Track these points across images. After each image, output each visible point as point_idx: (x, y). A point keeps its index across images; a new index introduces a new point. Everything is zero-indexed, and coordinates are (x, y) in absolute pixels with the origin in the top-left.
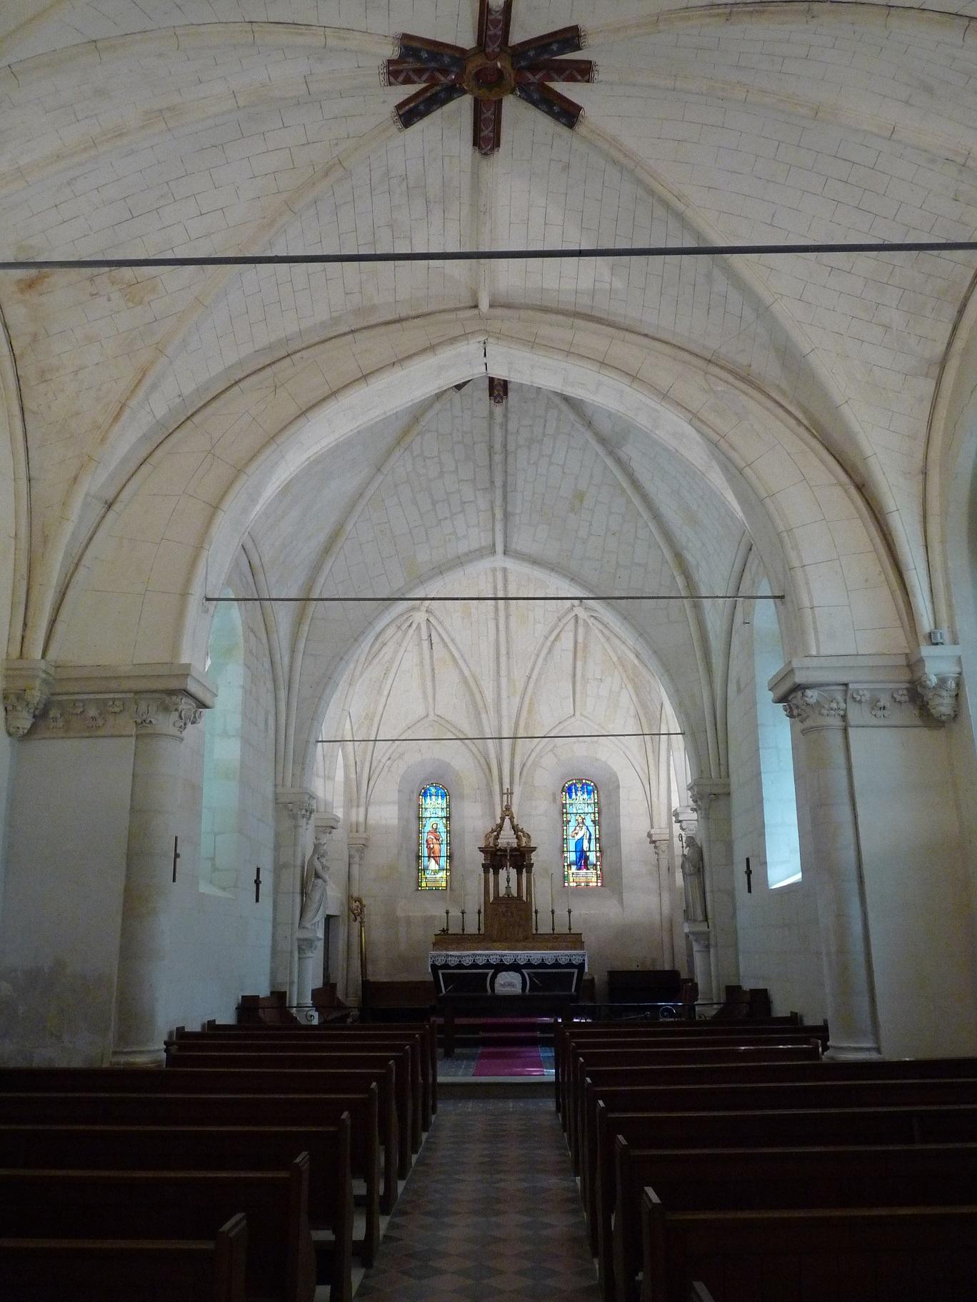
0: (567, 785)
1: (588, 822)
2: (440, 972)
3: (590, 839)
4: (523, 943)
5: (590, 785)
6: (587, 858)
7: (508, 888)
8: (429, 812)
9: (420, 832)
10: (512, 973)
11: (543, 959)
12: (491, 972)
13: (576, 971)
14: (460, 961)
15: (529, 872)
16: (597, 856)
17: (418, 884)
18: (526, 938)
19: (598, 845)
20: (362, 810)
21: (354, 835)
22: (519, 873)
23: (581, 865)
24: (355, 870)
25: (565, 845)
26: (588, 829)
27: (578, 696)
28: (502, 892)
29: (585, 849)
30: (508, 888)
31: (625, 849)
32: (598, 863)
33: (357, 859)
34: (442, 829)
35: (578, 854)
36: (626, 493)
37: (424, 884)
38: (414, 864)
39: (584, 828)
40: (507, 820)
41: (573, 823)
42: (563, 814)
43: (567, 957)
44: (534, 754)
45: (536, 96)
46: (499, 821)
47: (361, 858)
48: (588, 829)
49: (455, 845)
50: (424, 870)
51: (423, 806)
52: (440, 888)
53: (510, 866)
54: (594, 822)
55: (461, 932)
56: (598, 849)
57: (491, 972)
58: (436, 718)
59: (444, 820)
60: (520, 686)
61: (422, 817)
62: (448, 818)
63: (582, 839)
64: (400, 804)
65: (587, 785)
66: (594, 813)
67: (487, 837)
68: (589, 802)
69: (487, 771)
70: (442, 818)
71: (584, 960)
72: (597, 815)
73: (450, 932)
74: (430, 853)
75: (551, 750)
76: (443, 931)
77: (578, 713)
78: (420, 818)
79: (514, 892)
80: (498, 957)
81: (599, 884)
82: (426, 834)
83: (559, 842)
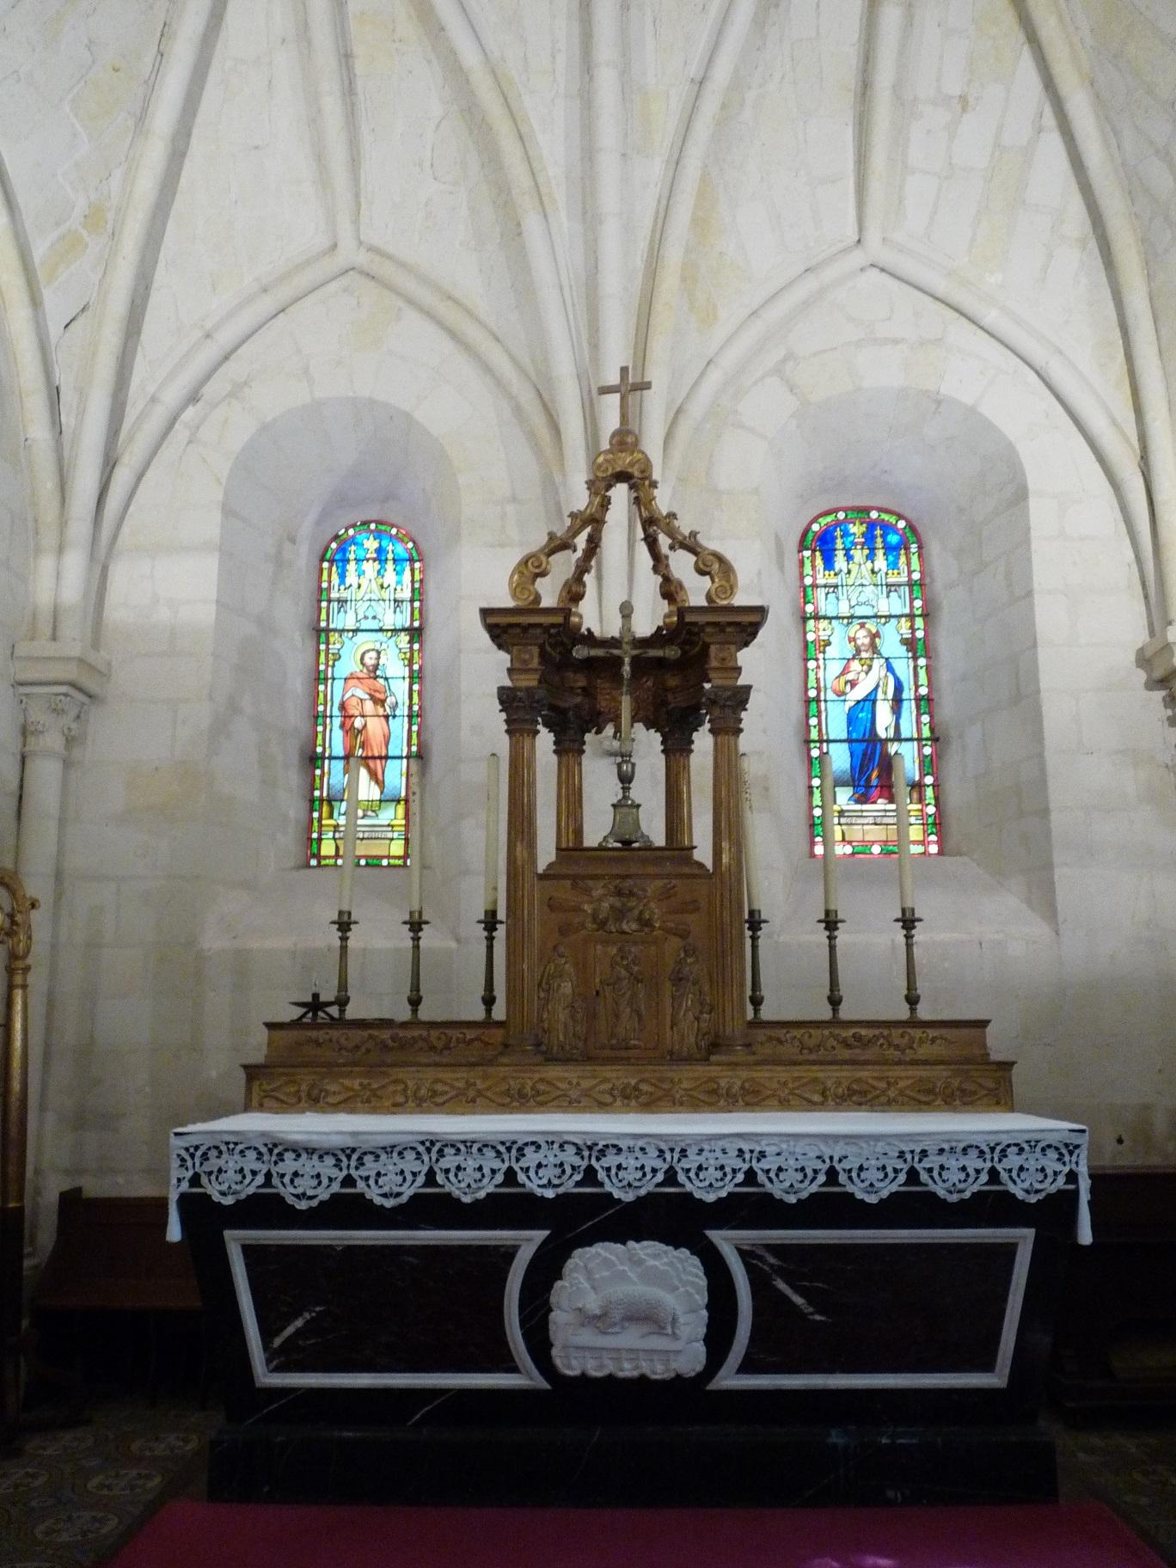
0: (815, 527)
1: (891, 644)
2: (235, 1240)
3: (897, 701)
4: (700, 1070)
5: (894, 528)
6: (888, 765)
7: (625, 806)
8: (351, 614)
9: (319, 678)
10: (652, 1253)
11: (832, 1174)
12: (529, 1241)
13: (1024, 1238)
14: (349, 1181)
15: (727, 729)
16: (922, 757)
17: (310, 845)
18: (714, 1045)
19: (925, 719)
20: (75, 563)
21: (43, 647)
22: (677, 749)
23: (868, 786)
24: (46, 776)
25: (813, 721)
26: (890, 668)
27: (876, 187)
28: (597, 828)
29: (882, 734)
30: (625, 806)
31: (1056, 712)
32: (929, 780)
33: (52, 740)
34: (394, 667)
35: (860, 748)
36: (702, 627)
37: (328, 848)
38: (293, 778)
39: (878, 664)
40: (620, 494)
41: (839, 649)
42: (805, 619)
43: (973, 1162)
44: (715, 377)
45: (614, 442)
46: (580, 499)
47: (70, 741)
48: (890, 668)
49: (433, 718)
50: (330, 801)
51: (334, 595)
52: (385, 862)
53: (634, 719)
54: (910, 644)
55: (825, 1013)
56: (926, 733)
57: (529, 1241)
58: (362, 259)
59: (404, 639)
60: (665, 117)
61: (327, 631)
62: (416, 633)
63: (871, 700)
64: (227, 553)
65: (887, 528)
66: (911, 617)
67: (531, 569)
68: (891, 580)
69: (544, 434)
70: (395, 631)
71: (1072, 1177)
72: (919, 622)
73: (352, 1012)
74: (353, 748)
75: (778, 370)
76: (315, 1005)
77: (873, 236)
78: (320, 633)
79: (654, 829)
80: (569, 1157)
81: (934, 849)
82: (339, 685)
83: (797, 709)
